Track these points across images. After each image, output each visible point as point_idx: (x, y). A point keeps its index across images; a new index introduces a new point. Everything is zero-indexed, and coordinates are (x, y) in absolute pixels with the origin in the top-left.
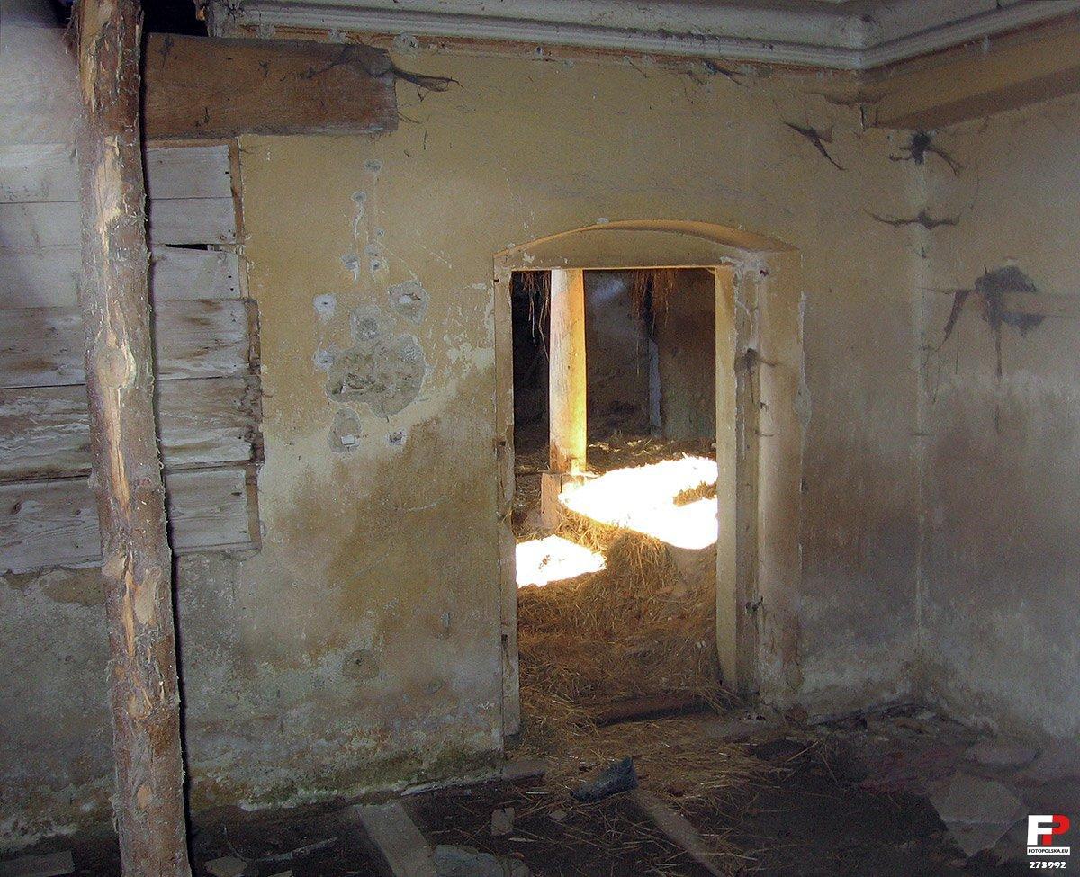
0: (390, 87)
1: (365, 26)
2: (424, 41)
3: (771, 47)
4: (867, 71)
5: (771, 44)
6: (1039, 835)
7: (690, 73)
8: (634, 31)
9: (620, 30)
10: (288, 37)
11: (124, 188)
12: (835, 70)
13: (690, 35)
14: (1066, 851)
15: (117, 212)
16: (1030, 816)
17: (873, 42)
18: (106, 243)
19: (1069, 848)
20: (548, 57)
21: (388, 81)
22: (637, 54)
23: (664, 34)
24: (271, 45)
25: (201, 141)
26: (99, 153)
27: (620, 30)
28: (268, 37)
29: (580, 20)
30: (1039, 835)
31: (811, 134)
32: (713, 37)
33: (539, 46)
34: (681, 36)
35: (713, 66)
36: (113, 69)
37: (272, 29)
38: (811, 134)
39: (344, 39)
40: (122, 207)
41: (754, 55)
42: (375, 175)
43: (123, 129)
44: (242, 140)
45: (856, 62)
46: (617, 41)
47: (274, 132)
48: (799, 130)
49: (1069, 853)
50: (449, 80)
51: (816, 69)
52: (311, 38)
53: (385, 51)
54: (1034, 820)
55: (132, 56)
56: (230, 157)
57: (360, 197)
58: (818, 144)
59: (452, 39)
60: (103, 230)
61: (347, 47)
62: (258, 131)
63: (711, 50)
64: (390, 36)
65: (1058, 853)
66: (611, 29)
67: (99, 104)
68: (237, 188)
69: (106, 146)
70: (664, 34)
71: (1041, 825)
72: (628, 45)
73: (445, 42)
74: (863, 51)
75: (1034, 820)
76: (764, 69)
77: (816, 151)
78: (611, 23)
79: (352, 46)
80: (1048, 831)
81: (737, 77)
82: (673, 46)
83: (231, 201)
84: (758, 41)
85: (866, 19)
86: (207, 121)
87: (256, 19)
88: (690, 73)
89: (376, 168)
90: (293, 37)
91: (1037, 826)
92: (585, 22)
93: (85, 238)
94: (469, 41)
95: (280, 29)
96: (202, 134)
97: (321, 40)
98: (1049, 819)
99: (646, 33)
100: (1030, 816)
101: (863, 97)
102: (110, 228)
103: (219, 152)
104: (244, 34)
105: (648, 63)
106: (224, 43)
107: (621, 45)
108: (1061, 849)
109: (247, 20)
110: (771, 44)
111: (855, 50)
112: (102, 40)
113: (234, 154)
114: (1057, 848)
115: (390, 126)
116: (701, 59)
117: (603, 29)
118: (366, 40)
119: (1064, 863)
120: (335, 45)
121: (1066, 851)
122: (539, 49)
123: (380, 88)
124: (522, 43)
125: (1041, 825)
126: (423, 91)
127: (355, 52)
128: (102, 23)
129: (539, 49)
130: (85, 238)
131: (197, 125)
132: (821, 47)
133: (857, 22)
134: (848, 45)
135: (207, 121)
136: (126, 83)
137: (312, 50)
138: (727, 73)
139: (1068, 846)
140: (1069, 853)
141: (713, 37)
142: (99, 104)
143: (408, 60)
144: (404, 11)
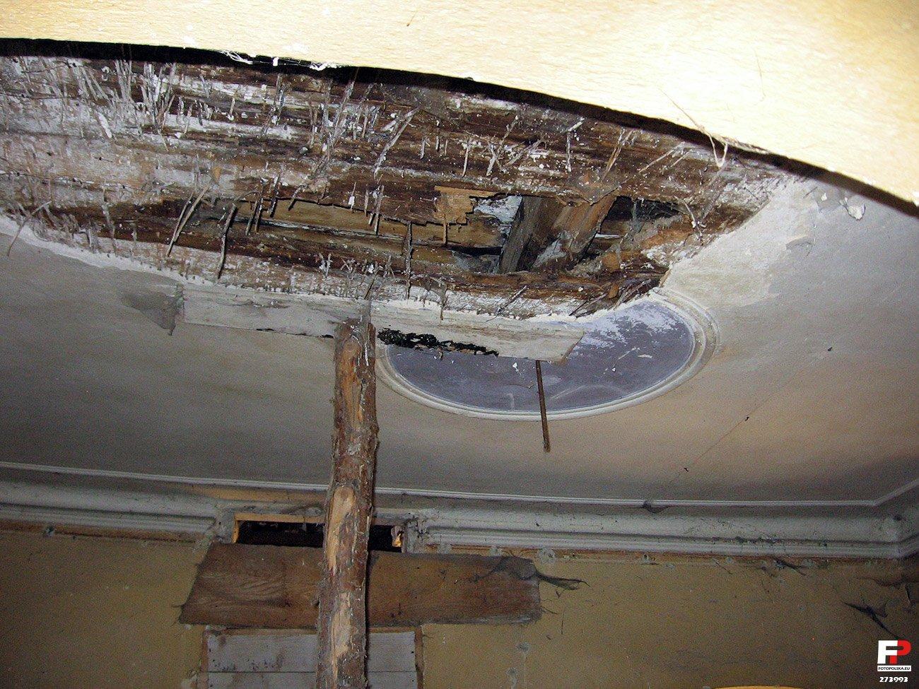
0: (535, 587)
1: (515, 543)
2: (560, 553)
3: (826, 545)
4: (906, 558)
5: (825, 543)
6: (887, 656)
7: (764, 569)
8: (717, 539)
9: (706, 539)
10: (460, 552)
11: (352, 631)
12: (879, 559)
13: (760, 540)
14: (908, 668)
15: (345, 649)
16: (879, 641)
17: (906, 536)
18: (336, 673)
19: (910, 666)
20: (653, 562)
21: (534, 583)
22: (721, 556)
23: (741, 540)
24: (447, 558)
25: (395, 628)
26: (335, 604)
27: (706, 539)
28: (445, 553)
29: (675, 534)
30: (887, 656)
31: (869, 611)
32: (779, 541)
33: (645, 554)
34: (754, 541)
35: (782, 562)
36: (350, 546)
37: (449, 547)
38: (869, 611)
39: (500, 553)
40: (349, 645)
41: (815, 552)
42: (524, 655)
43: (354, 588)
44: (424, 628)
45: (895, 552)
46: (704, 548)
47: (449, 622)
48: (860, 609)
49: (910, 670)
50: (579, 581)
51: (864, 560)
52: (476, 552)
53: (530, 561)
54: (882, 644)
55: (363, 537)
56: (416, 640)
57: (513, 672)
58: (874, 619)
59: (580, 551)
60: (334, 662)
61: (504, 558)
62: (436, 621)
63: (778, 550)
64: (534, 550)
65: (902, 670)
66: (700, 539)
67: (339, 570)
68: (419, 665)
69: (341, 600)
70: (741, 540)
71: (888, 648)
72: (713, 550)
73: (575, 553)
74: (901, 543)
75: (882, 644)
76: (823, 563)
77: (874, 624)
78: (699, 534)
79: (506, 558)
80: (894, 653)
81: (801, 570)
82: (748, 549)
83: (415, 675)
84: (815, 541)
85: (898, 518)
86: (400, 613)
87: (437, 540)
88: (764, 569)
89: (525, 649)
90: (464, 552)
91: (885, 649)
92: (679, 535)
93: (321, 668)
94: (593, 551)
95: (455, 546)
96: (396, 623)
97: (484, 554)
98: (894, 643)
99: (726, 540)
100: (879, 641)
101: (905, 579)
102: (340, 661)
103: (408, 636)
104: (429, 550)
105: (730, 563)
106: (415, 557)
107: (707, 550)
108: (904, 667)
109: (431, 541)
110: (825, 543)
111: (892, 543)
112: (344, 525)
113: (419, 638)
114: (901, 667)
115: (536, 616)
116: (771, 557)
117: (693, 539)
118: (516, 553)
119: (906, 678)
120: (493, 557)
121: (908, 668)
122: (646, 556)
123: (528, 587)
124: (633, 552)
125: (888, 648)
126: (560, 589)
127: (508, 562)
128: (345, 514)
129: (646, 556)
130: (321, 668)
131: (393, 616)
132: (865, 543)
133: (890, 521)
134: (886, 539)
135: (400, 613)
136: (358, 556)
137: (478, 561)
138: (794, 567)
139: (909, 665)
140: (910, 670)
141: (779, 541)
142: (339, 570)
143: (548, 567)
144: (544, 532)
